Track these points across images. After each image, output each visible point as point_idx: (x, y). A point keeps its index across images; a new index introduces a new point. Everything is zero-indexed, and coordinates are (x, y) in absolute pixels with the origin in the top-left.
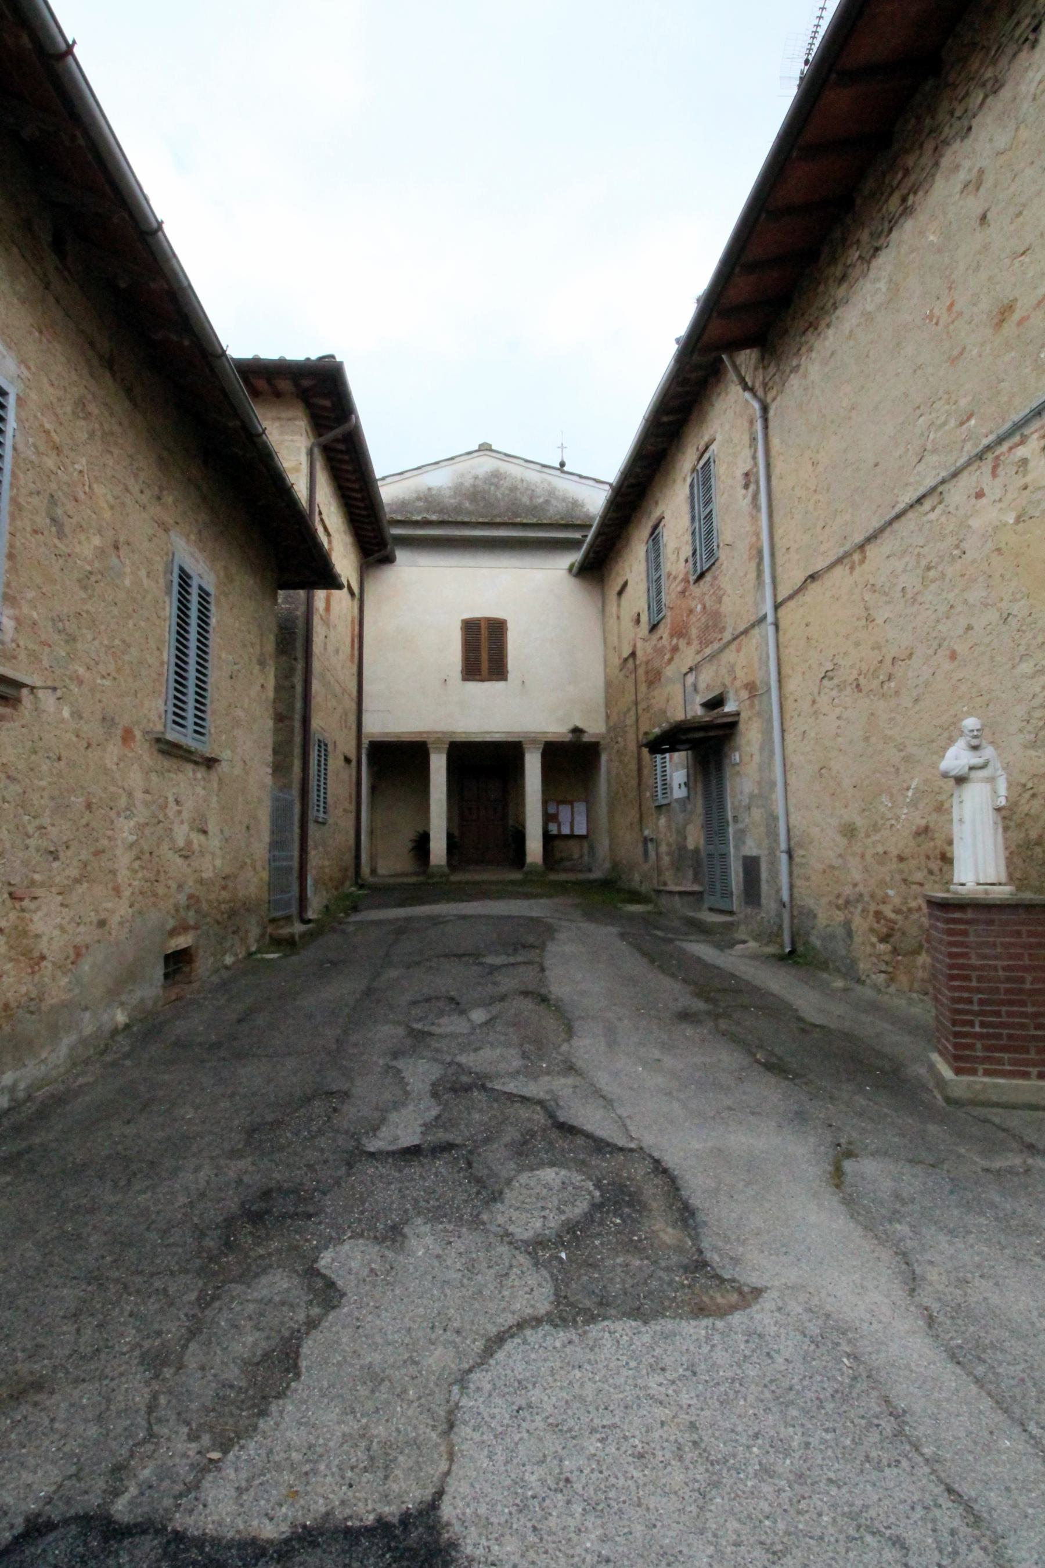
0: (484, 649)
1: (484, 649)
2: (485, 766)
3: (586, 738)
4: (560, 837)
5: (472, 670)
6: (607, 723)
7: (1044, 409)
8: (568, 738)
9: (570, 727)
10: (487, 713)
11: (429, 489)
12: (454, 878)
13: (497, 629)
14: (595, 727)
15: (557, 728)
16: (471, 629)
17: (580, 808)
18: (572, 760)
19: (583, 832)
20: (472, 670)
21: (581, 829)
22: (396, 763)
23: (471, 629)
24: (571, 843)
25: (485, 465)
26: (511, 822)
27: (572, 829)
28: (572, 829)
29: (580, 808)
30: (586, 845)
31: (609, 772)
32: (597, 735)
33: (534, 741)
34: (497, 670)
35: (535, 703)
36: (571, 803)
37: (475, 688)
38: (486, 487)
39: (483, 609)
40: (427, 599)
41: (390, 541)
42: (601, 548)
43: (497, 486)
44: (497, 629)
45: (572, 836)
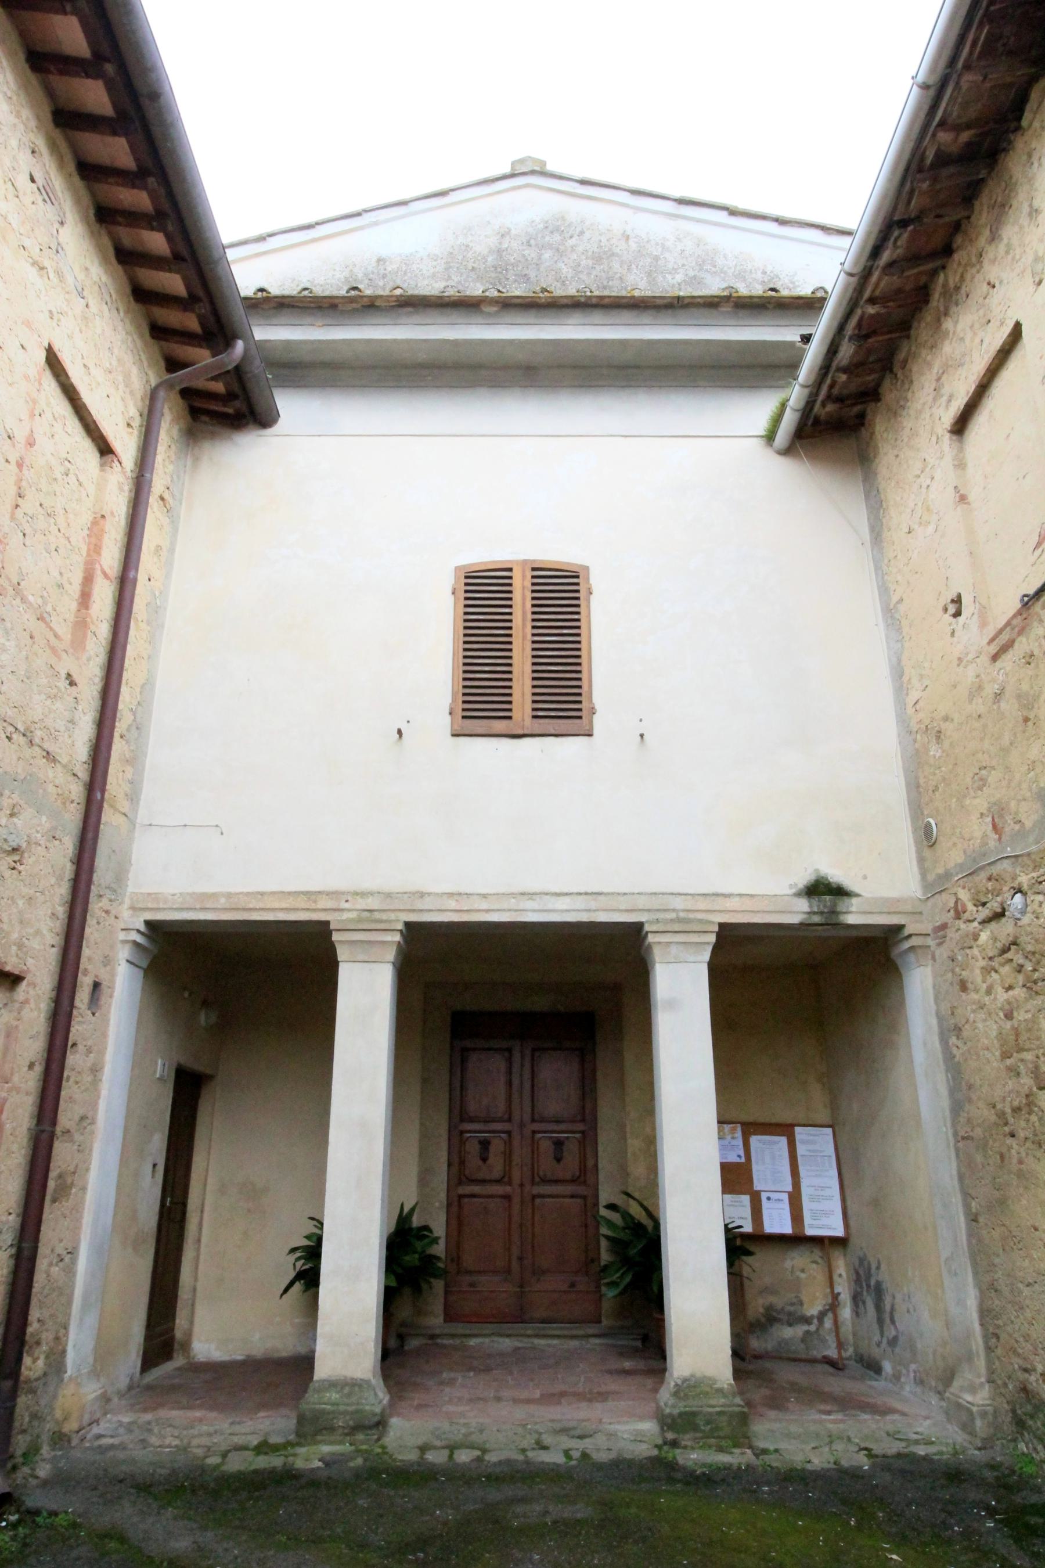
0: (523, 652)
1: (523, 652)
2: (524, 1014)
3: (855, 915)
4: (762, 1239)
5: (482, 703)
6: (923, 873)
7: (1044, 590)
8: (797, 912)
9: (803, 878)
10: (525, 840)
11: (380, 260)
12: (407, 1435)
13: (560, 593)
14: (883, 884)
15: (767, 891)
16: (484, 594)
17: (817, 1144)
18: (807, 989)
19: (836, 1228)
20: (482, 703)
21: (825, 1219)
22: (241, 990)
23: (484, 594)
24: (798, 1260)
25: (528, 208)
26: (607, 1194)
27: (797, 1216)
28: (797, 1216)
29: (817, 1144)
30: (841, 1267)
31: (951, 1030)
32: (890, 905)
33: (683, 925)
34: (563, 702)
35: (671, 816)
36: (786, 1130)
37: (490, 754)
38: (531, 254)
39: (520, 540)
40: (357, 519)
41: (239, 311)
42: (852, 387)
43: (559, 252)
44: (560, 593)
45: (797, 1240)
